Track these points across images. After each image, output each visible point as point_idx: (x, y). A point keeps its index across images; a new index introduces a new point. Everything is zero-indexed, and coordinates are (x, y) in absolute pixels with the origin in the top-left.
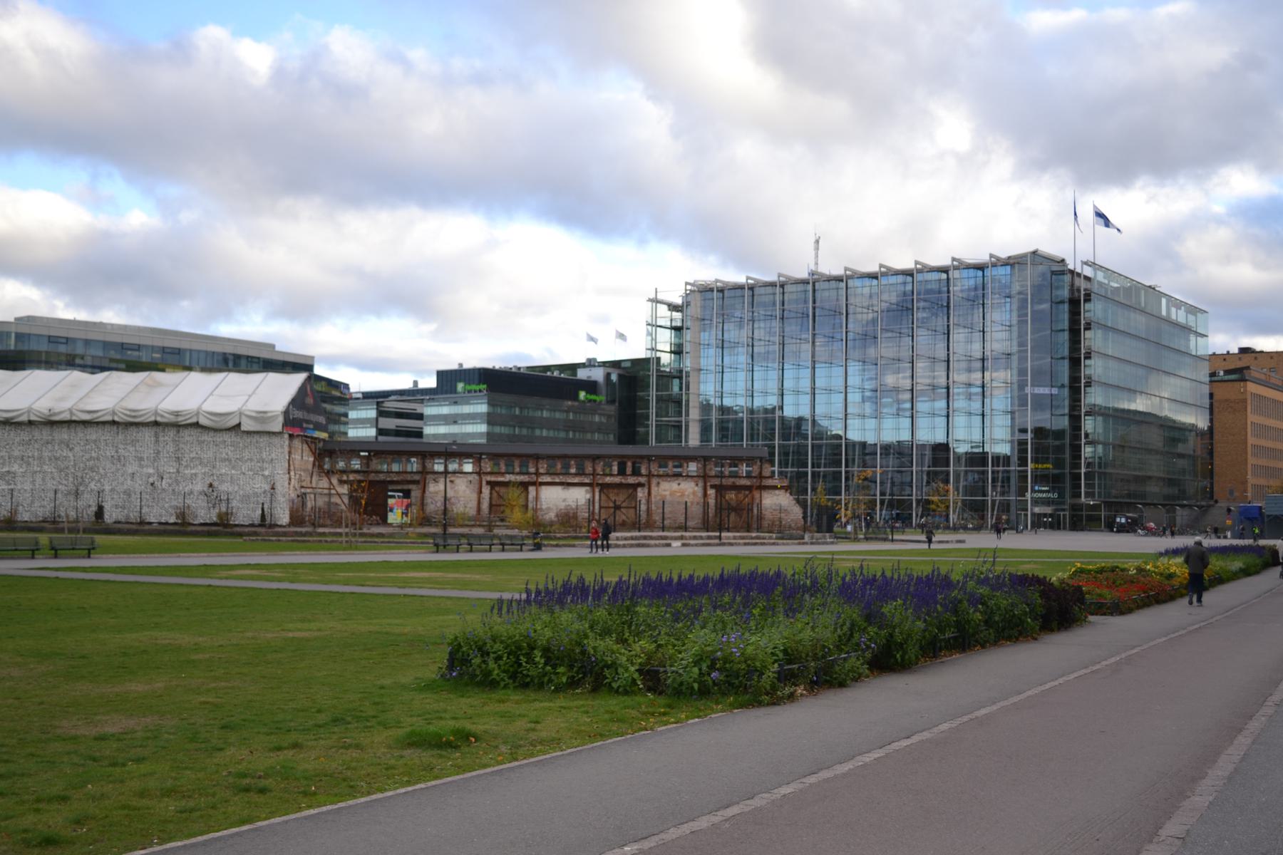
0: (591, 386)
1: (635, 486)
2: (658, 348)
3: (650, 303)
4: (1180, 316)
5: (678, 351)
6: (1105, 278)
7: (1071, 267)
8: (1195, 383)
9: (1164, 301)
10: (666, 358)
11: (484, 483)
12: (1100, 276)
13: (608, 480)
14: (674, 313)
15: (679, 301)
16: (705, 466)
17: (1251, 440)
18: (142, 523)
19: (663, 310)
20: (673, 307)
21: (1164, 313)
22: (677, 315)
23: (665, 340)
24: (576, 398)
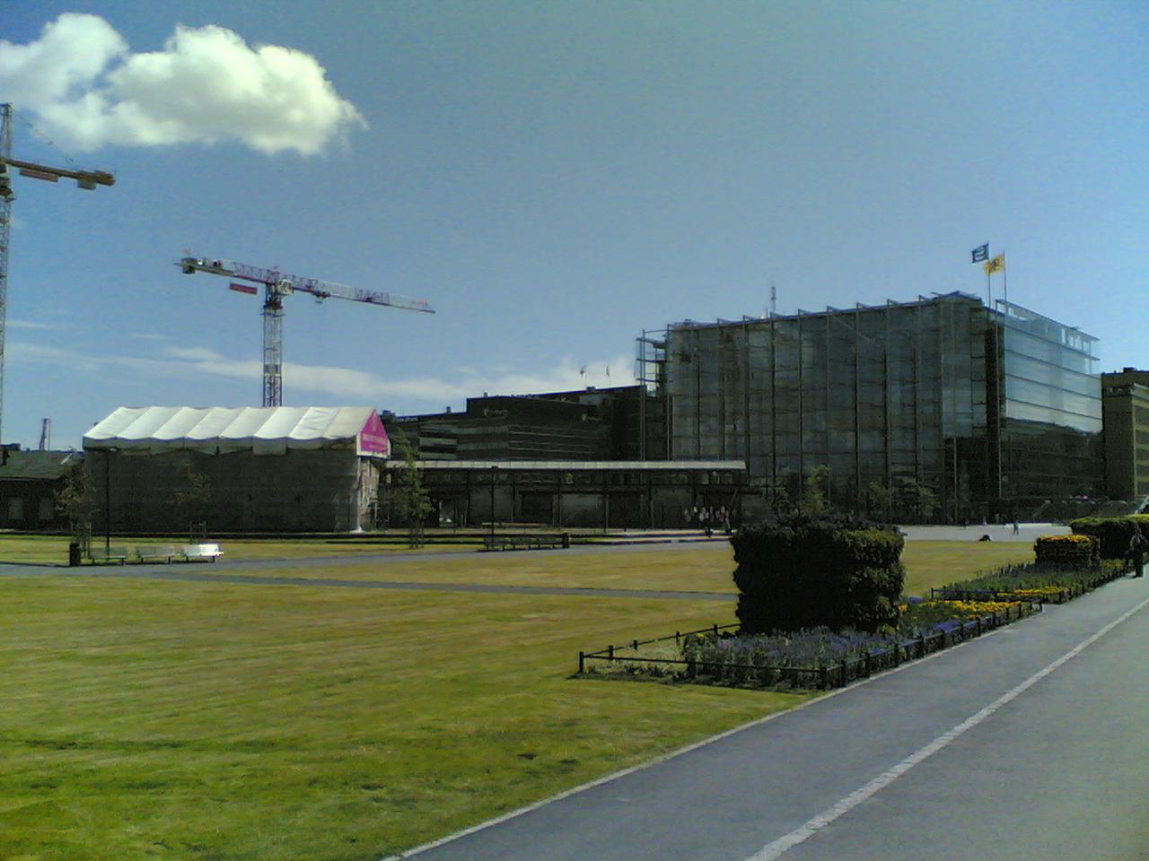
0: (591, 410)
1: (637, 494)
2: (646, 378)
3: (639, 342)
4: (1075, 343)
5: (661, 379)
6: (1015, 313)
7: (986, 305)
8: (1051, 410)
9: (1063, 331)
10: (651, 387)
11: (517, 492)
12: (1011, 312)
13: (617, 488)
14: (658, 350)
15: (662, 340)
16: (911, 451)
17: (1136, 446)
18: (370, 513)
19: (649, 347)
20: (657, 345)
21: (1064, 341)
22: (661, 351)
23: (651, 370)
24: (579, 418)
